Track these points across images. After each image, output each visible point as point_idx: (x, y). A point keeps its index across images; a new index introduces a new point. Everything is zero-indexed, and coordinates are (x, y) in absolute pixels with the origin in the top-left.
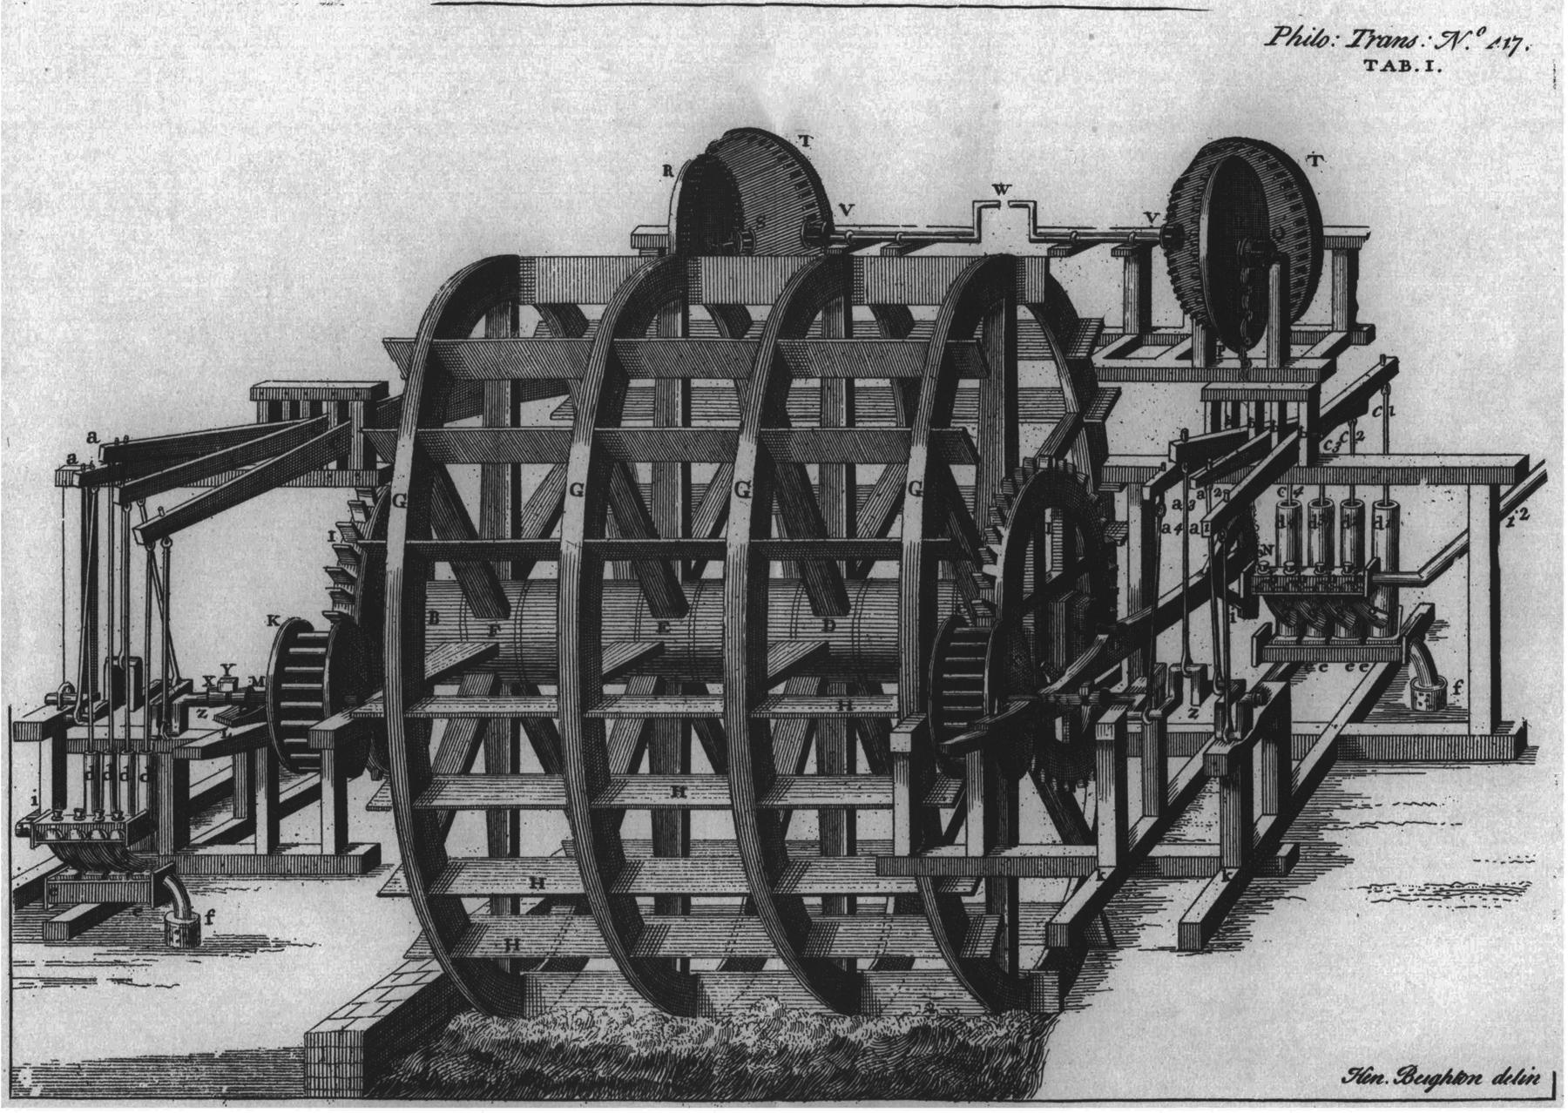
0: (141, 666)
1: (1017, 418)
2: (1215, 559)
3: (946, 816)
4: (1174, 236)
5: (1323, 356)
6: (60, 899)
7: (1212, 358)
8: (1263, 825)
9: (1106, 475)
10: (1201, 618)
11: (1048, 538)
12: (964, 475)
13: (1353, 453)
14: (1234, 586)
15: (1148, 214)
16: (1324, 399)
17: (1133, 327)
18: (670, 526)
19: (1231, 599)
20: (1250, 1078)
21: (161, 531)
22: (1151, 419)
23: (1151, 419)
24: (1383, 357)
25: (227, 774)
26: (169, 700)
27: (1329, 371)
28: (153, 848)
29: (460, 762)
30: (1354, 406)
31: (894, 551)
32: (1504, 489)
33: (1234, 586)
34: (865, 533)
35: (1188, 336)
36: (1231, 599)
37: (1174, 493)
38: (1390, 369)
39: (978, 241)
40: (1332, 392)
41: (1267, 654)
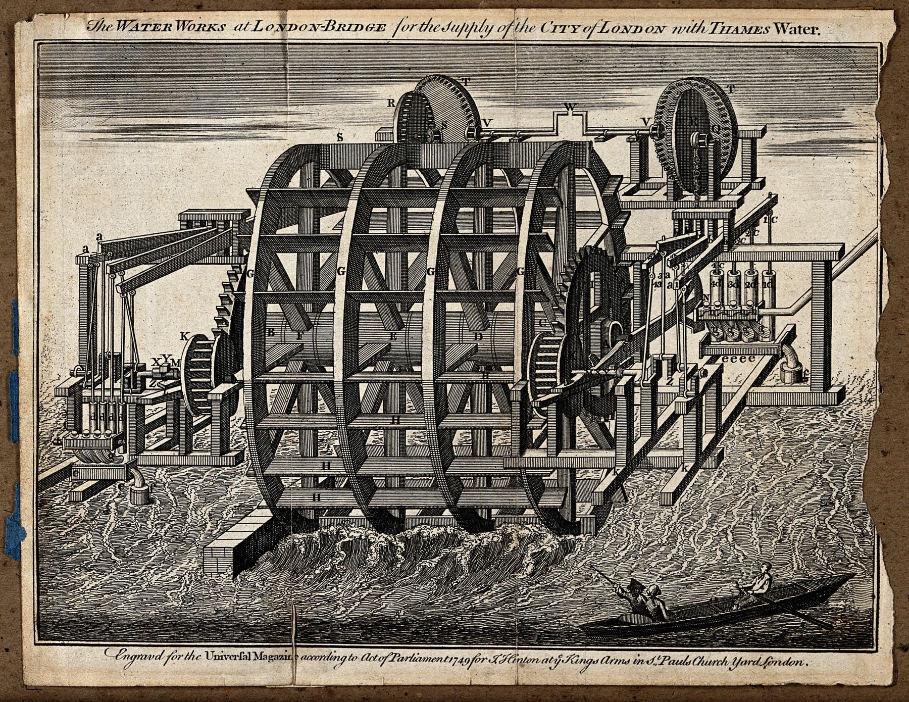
0: (119, 358)
1: (574, 193)
2: (679, 303)
3: (536, 434)
4: (659, 132)
5: (739, 194)
6: (79, 476)
7: (677, 196)
8: (707, 439)
9: (624, 257)
10: (671, 334)
11: (592, 290)
12: (547, 258)
13: (752, 243)
14: (690, 316)
15: (644, 119)
16: (737, 218)
17: (636, 176)
18: (395, 286)
19: (689, 322)
20: (63, 33)
21: (129, 288)
22: (648, 228)
23: (648, 228)
24: (770, 194)
25: (164, 413)
26: (133, 376)
27: (740, 202)
28: (668, 480)
29: (286, 405)
30: (751, 224)
31: (511, 298)
32: (834, 263)
33: (690, 316)
34: (497, 287)
35: (664, 184)
36: (689, 322)
37: (658, 268)
38: (774, 200)
39: (557, 135)
40: (741, 215)
41: (706, 351)
